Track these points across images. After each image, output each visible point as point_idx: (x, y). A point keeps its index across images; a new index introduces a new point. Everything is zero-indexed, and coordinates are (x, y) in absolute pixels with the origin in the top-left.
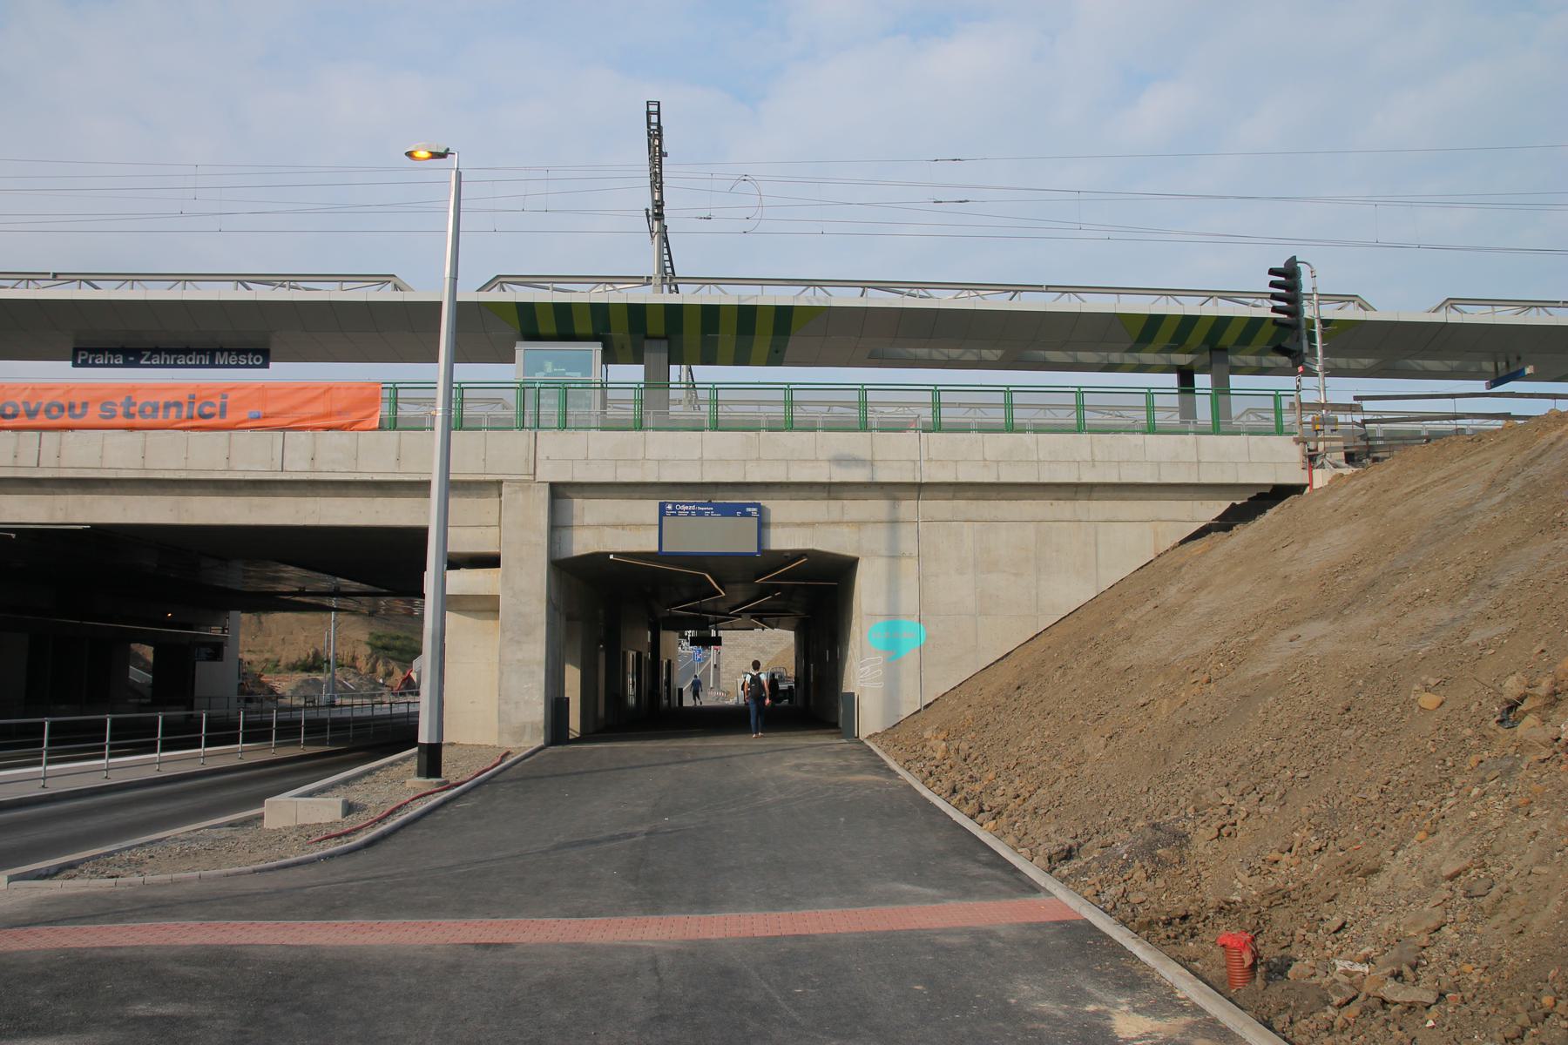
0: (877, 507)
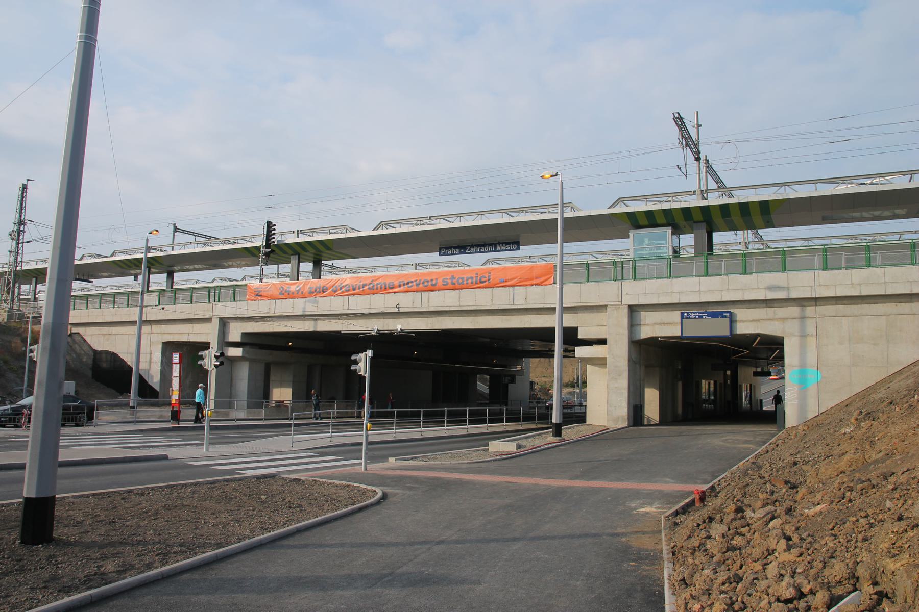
0: (794, 311)
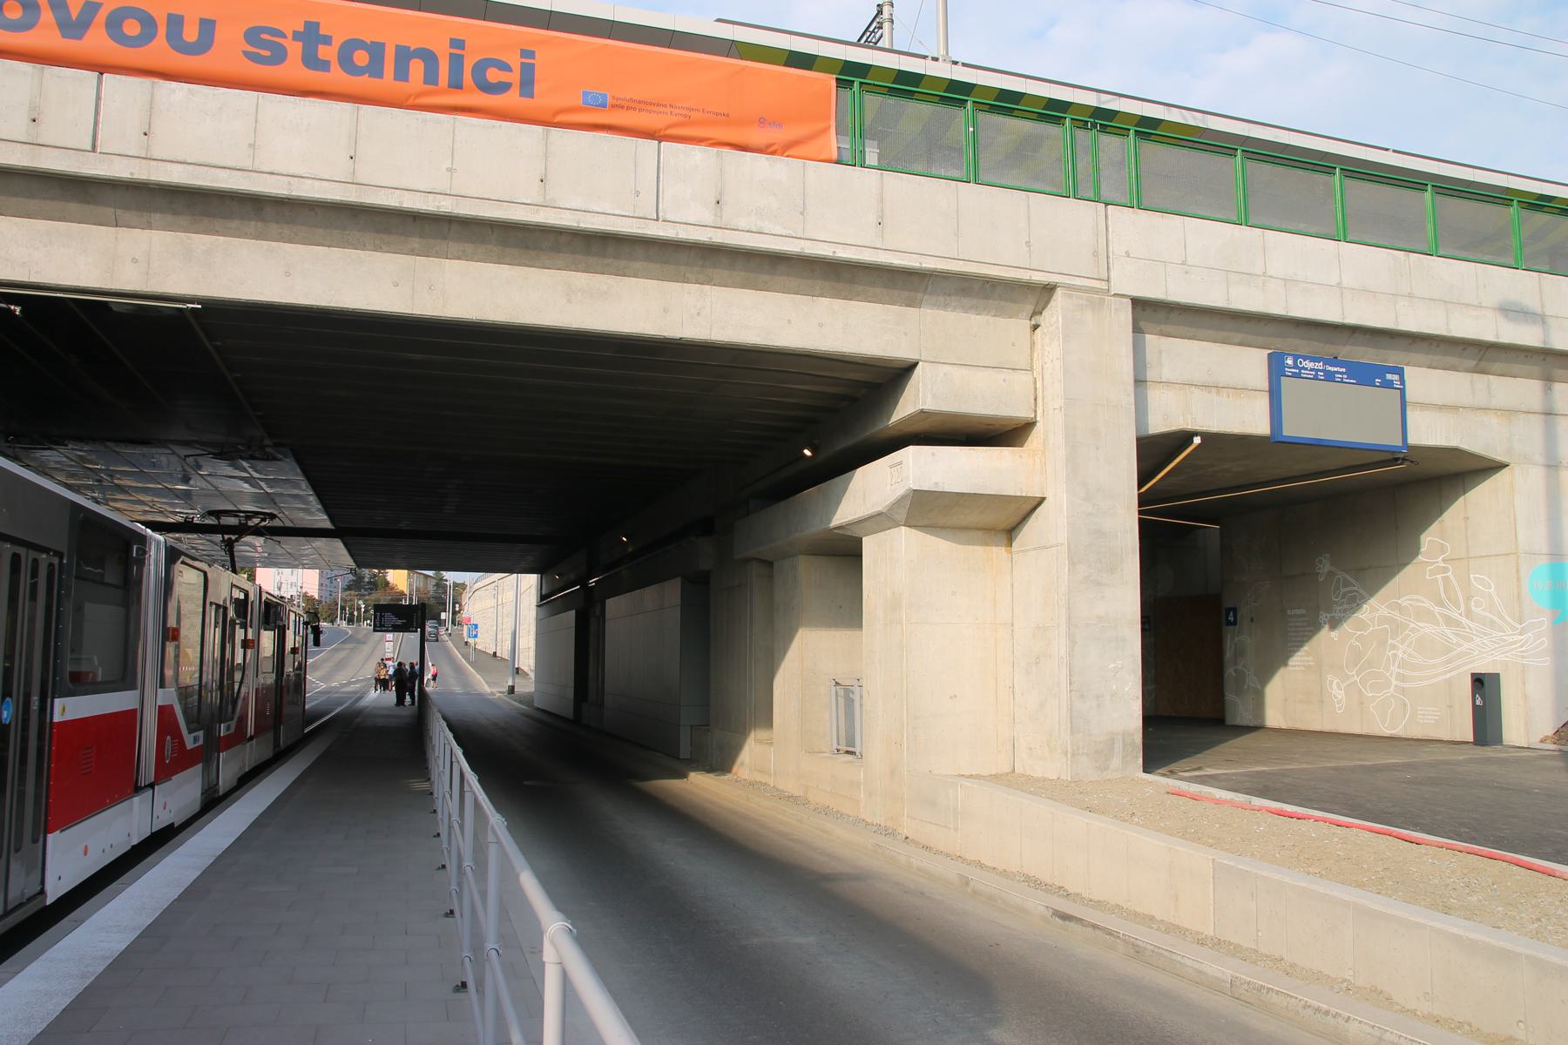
0: (1522, 390)
